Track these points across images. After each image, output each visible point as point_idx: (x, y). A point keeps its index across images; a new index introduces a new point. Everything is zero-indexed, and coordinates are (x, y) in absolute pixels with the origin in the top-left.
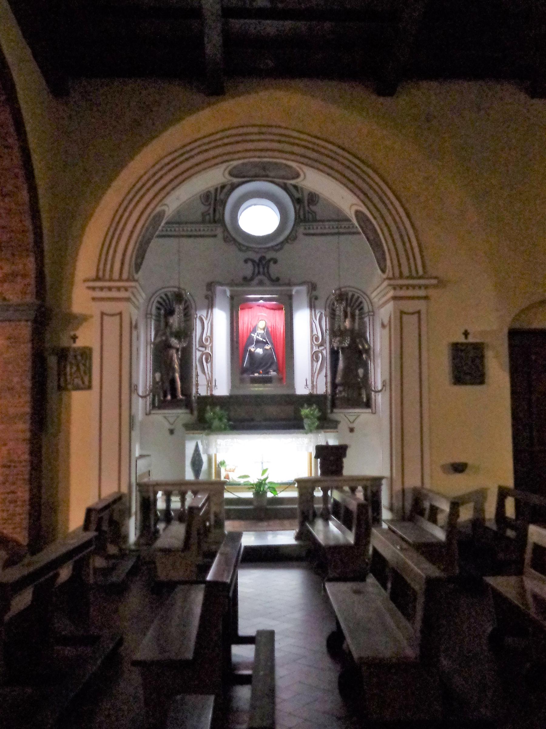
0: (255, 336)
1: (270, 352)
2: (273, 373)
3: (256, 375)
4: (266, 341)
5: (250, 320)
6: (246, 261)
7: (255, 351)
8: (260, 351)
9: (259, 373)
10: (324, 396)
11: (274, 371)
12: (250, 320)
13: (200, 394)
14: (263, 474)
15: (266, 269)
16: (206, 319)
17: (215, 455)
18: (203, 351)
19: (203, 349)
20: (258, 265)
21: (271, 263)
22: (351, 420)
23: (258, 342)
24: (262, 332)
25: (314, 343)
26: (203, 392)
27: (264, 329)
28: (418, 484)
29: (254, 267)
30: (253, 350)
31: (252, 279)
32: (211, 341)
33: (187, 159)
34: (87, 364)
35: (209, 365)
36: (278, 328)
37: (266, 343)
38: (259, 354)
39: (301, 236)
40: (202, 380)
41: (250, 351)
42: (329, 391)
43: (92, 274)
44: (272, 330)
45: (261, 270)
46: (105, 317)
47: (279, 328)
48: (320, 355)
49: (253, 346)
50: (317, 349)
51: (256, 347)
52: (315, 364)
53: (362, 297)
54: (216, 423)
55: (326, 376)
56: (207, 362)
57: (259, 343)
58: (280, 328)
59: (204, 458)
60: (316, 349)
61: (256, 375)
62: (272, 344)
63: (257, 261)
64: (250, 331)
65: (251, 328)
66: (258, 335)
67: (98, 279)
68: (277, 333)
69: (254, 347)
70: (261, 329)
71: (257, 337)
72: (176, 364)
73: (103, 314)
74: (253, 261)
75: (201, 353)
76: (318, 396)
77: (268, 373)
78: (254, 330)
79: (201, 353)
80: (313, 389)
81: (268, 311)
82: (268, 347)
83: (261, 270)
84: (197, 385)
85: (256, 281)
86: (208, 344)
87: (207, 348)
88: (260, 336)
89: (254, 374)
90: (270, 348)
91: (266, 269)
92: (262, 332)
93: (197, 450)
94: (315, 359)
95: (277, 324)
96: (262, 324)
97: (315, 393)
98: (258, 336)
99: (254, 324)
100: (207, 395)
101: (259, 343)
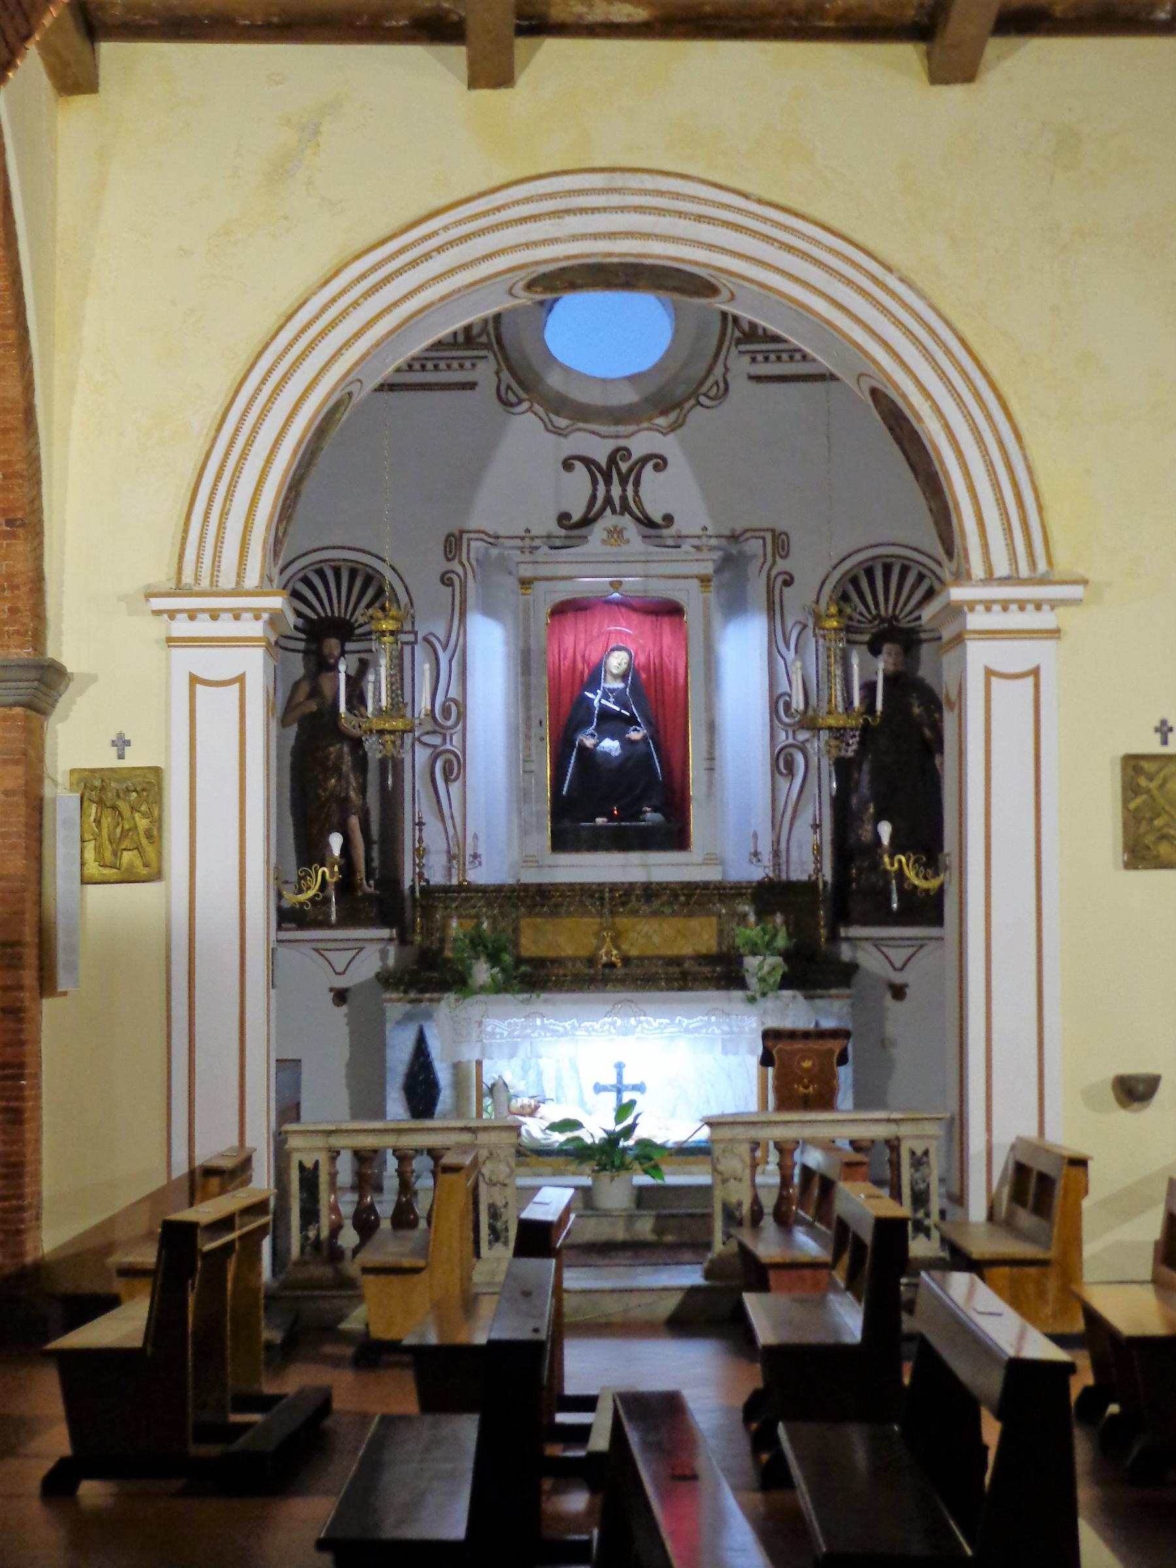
0: (596, 699)
1: (641, 748)
2: (652, 817)
3: (600, 821)
4: (632, 714)
5: (582, 644)
6: (567, 465)
7: (596, 745)
8: (611, 745)
9: (611, 818)
10: (810, 887)
11: (655, 810)
12: (582, 644)
13: (427, 881)
14: (619, 1118)
15: (630, 488)
16: (445, 648)
17: (479, 1064)
18: (435, 747)
19: (436, 740)
20: (608, 482)
21: (649, 466)
22: (898, 964)
23: (606, 715)
24: (619, 685)
25: (780, 721)
26: (436, 876)
27: (624, 677)
28: (1030, 1131)
29: (594, 482)
30: (589, 742)
31: (587, 521)
32: (462, 716)
33: (414, 264)
34: (156, 814)
35: (455, 788)
36: (669, 671)
37: (631, 721)
38: (607, 755)
39: (740, 387)
40: (434, 838)
41: (583, 748)
42: (828, 873)
43: (160, 574)
44: (649, 677)
45: (616, 491)
46: (199, 688)
47: (672, 671)
48: (800, 759)
49: (591, 730)
50: (791, 741)
51: (602, 734)
52: (783, 784)
53: (933, 578)
54: (482, 972)
55: (816, 826)
56: (447, 780)
57: (610, 722)
58: (676, 673)
59: (444, 1076)
60: (787, 737)
61: (600, 821)
62: (649, 724)
63: (604, 464)
64: (582, 680)
65: (582, 673)
66: (605, 696)
67: (180, 591)
68: (666, 678)
69: (592, 735)
70: (615, 677)
71: (603, 701)
72: (351, 788)
73: (194, 680)
74: (588, 462)
75: (429, 751)
76: (791, 887)
77: (637, 815)
78: (594, 681)
79: (429, 751)
80: (776, 865)
81: (635, 618)
82: (635, 735)
83: (616, 491)
84: (419, 852)
85: (598, 531)
86: (449, 723)
87: (448, 738)
88: (612, 700)
89: (593, 821)
90: (645, 738)
91: (630, 488)
92: (619, 685)
93: (421, 1050)
94: (784, 771)
95: (666, 659)
96: (617, 662)
97: (784, 877)
98: (607, 698)
99: (594, 658)
100: (448, 883)
101: (610, 722)
